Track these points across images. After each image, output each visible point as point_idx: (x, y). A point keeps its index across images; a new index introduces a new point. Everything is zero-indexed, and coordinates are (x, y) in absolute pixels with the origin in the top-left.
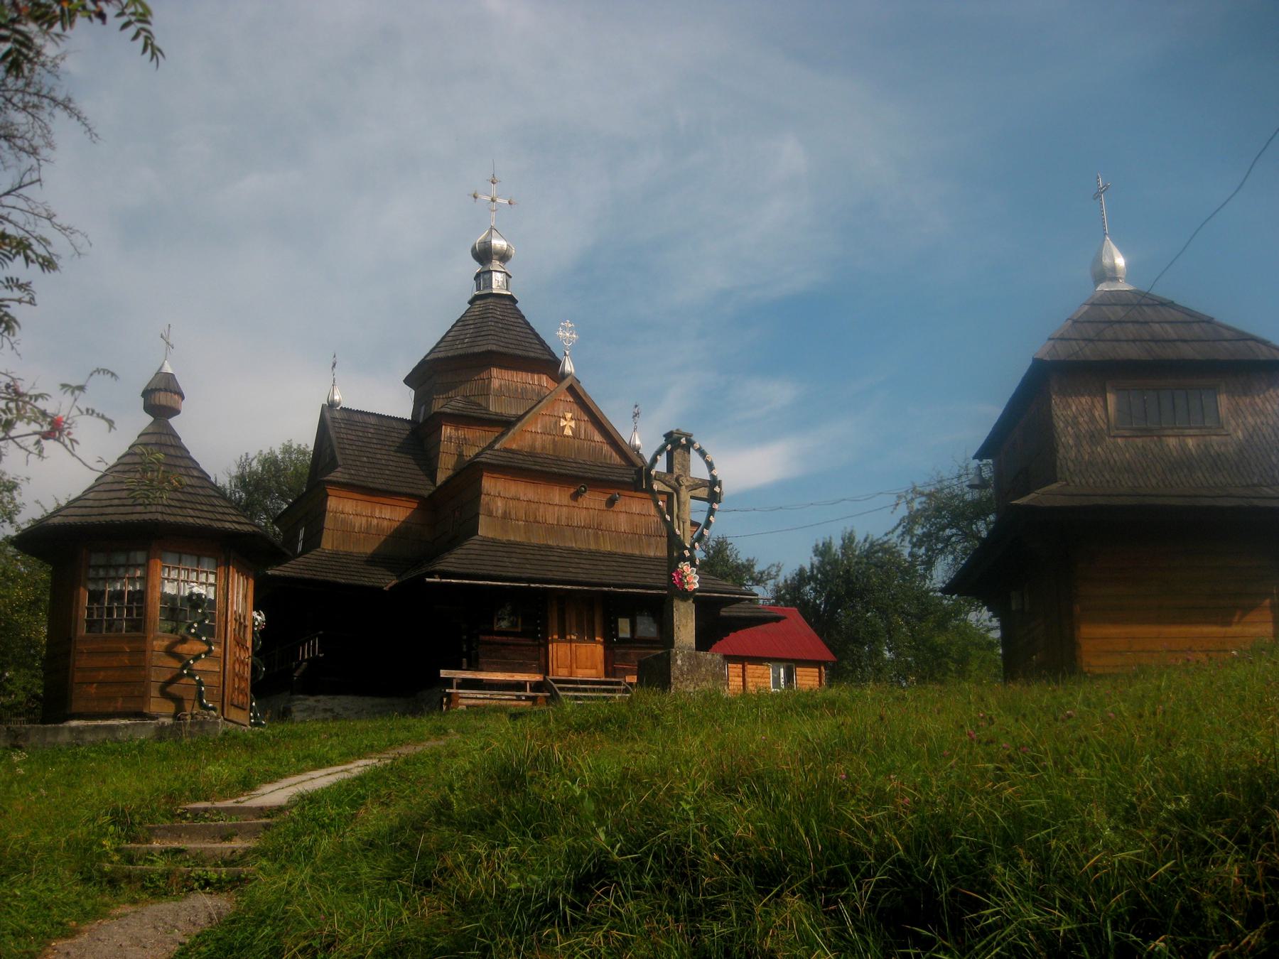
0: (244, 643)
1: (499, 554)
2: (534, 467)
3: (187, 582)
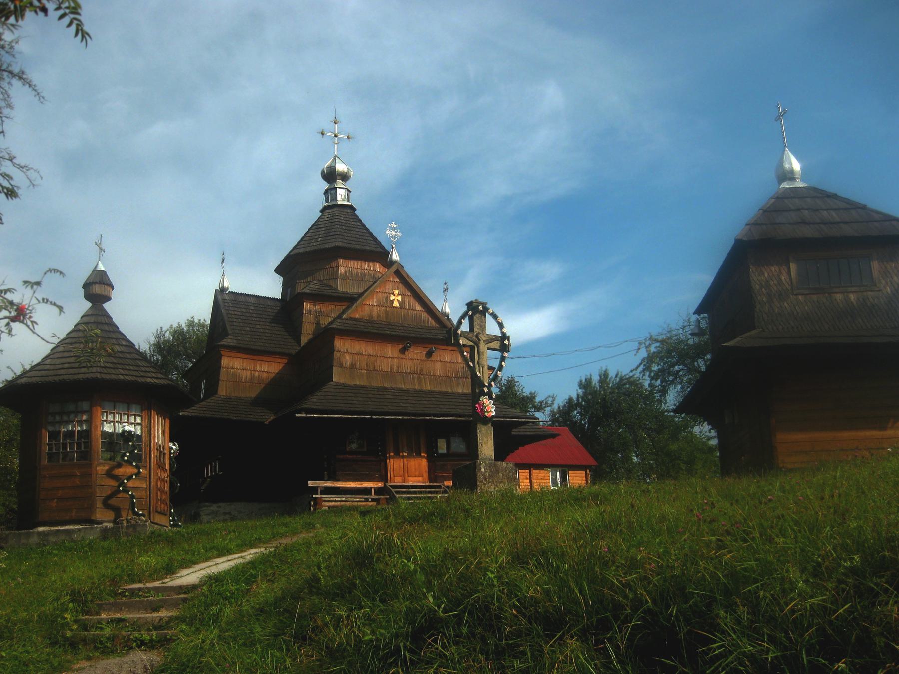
2: (372, 330)
3: (121, 423)
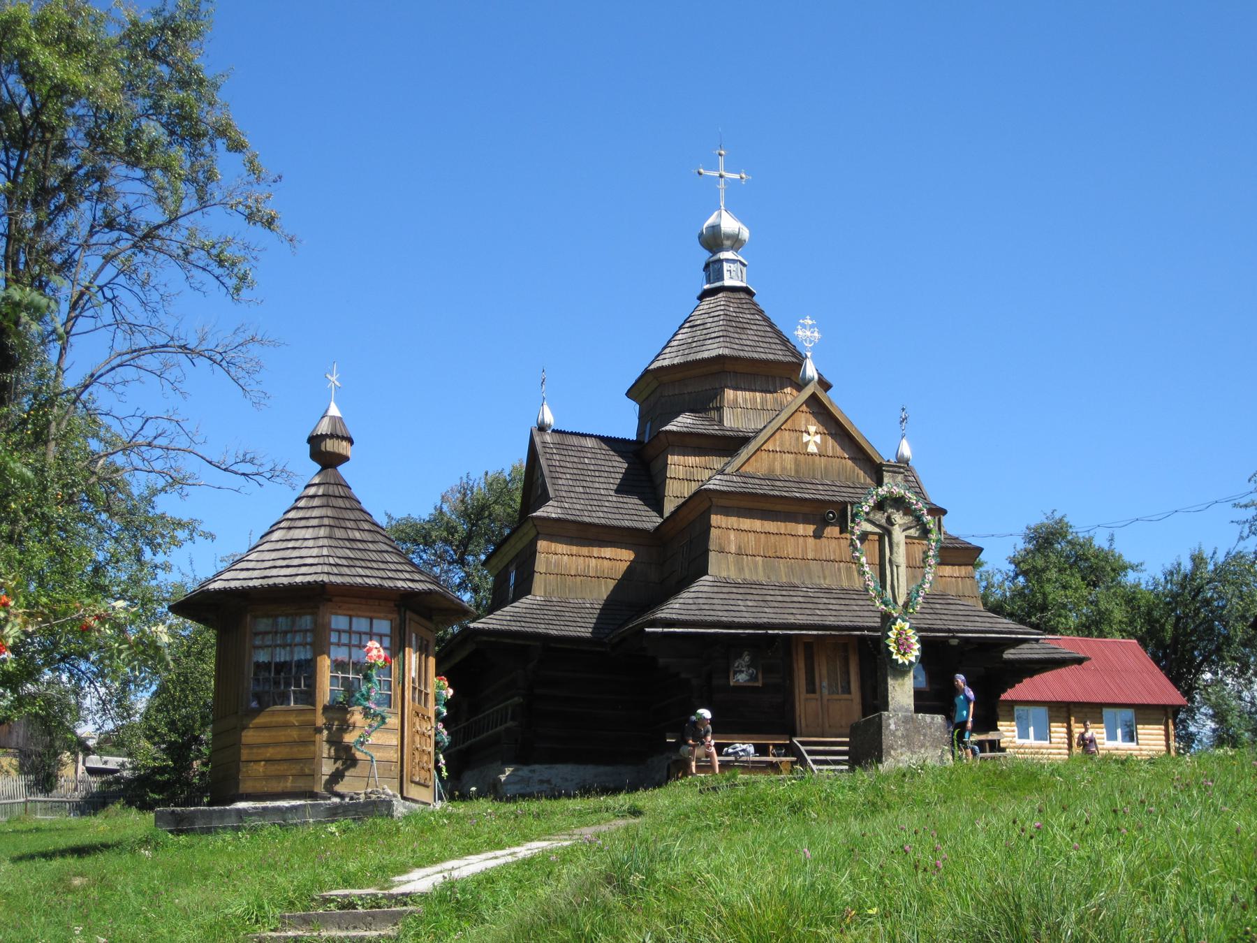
0: (424, 713)
1: (733, 596)
2: (771, 493)
